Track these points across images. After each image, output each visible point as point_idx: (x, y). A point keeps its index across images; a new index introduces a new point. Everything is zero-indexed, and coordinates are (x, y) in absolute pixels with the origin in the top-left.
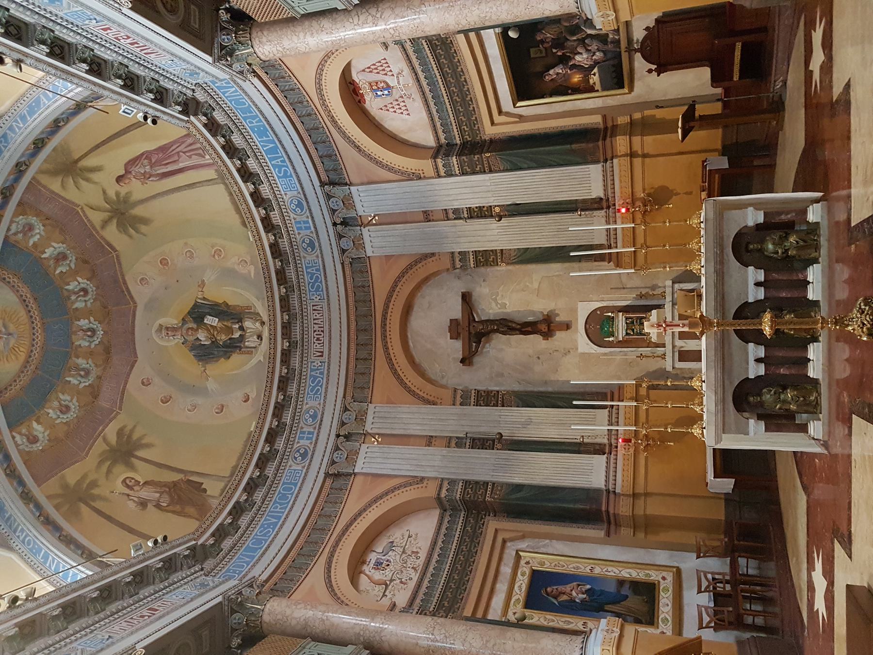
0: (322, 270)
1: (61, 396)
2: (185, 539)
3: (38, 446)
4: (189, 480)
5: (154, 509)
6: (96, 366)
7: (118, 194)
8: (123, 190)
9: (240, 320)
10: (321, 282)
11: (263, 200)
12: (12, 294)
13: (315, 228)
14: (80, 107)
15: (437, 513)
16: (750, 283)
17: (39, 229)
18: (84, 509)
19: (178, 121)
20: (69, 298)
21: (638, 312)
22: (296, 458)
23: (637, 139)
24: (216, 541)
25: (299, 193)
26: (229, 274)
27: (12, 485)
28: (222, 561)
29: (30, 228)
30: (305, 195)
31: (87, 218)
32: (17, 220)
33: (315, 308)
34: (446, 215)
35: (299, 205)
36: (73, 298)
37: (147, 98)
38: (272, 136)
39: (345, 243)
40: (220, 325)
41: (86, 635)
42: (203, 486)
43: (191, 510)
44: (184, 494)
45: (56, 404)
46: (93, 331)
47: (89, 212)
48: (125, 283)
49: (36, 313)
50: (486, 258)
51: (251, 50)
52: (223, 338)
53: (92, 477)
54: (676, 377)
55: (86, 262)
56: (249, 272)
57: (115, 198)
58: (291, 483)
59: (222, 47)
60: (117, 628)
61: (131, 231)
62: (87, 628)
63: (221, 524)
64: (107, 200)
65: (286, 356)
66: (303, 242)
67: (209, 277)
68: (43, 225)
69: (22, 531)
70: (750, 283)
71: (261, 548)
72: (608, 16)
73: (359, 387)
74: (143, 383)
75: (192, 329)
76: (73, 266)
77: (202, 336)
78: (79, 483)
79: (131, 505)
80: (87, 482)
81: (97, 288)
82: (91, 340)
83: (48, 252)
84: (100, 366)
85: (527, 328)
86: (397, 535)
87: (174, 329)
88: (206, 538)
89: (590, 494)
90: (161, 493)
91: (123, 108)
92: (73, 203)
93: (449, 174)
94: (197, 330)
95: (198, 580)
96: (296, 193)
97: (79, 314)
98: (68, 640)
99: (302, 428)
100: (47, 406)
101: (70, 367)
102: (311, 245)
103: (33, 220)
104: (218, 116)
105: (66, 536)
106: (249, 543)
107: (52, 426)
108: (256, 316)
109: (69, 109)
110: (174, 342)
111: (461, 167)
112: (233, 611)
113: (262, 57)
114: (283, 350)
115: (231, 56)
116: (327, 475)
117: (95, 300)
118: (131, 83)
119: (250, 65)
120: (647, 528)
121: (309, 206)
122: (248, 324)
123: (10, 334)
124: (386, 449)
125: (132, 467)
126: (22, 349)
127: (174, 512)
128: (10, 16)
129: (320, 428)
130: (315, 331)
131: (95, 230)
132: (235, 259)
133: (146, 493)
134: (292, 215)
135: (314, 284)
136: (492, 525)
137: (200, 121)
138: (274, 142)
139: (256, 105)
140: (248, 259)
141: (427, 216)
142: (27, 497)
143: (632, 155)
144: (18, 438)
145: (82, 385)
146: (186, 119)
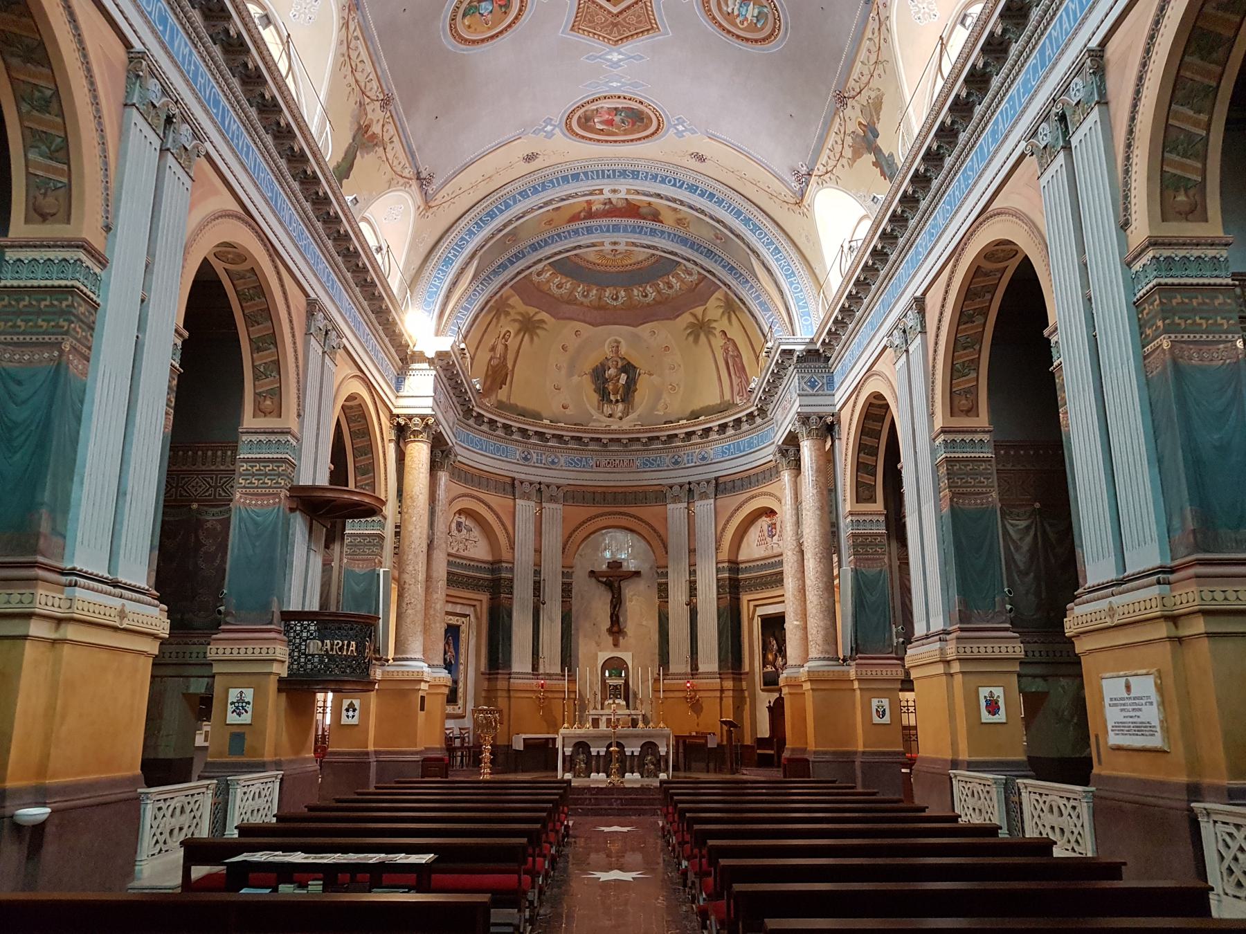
8: (717, 332)
15: (490, 558)
16: (633, 749)
21: (625, 693)
23: (731, 693)
26: (658, 397)
34: (692, 565)
35: (704, 458)
39: (676, 488)
46: (616, 299)
50: (663, 590)
54: (581, 716)
70: (633, 749)
72: (1112, 617)
73: (574, 495)
77: (612, 371)
78: (510, 306)
85: (615, 619)
86: (476, 533)
87: (617, 352)
89: (508, 664)
93: (718, 570)
102: (676, 463)
108: (626, 413)
110: (607, 351)
111: (722, 579)
112: (443, 452)
116: (513, 479)
120: (489, 696)
122: (621, 406)
124: (532, 520)
133: (500, 348)
136: (484, 597)
141: (692, 551)
143: (722, 691)
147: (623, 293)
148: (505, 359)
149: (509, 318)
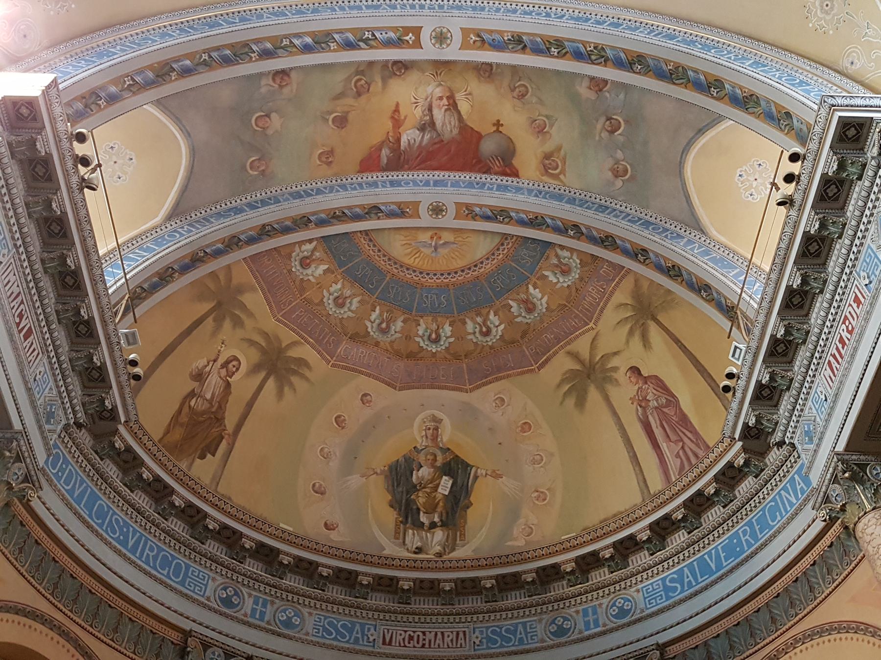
0: (521, 648)
1: (355, 301)
2: (130, 408)
3: (296, 266)
4: (223, 438)
5: (190, 389)
6: (392, 342)
7: (615, 369)
8: (621, 376)
9: (444, 525)
10: (502, 646)
11: (625, 558)
12: (484, 253)
13: (588, 638)
14: (730, 311)
17: (565, 281)
18: (207, 306)
19: (731, 424)
20: (479, 314)
22: (225, 589)
24: (119, 453)
25: (643, 611)
26: (513, 513)
27: (251, 229)
28: (85, 457)
29: (566, 272)
30: (639, 620)
31: (580, 334)
32: (575, 257)
33: (461, 635)
35: (623, 613)
36: (479, 320)
37: (760, 374)
38: (727, 565)
40: (439, 497)
41: (13, 238)
42: (209, 456)
43: (177, 435)
44: (203, 428)
45: (347, 292)
46: (437, 341)
47: (587, 338)
48: (498, 379)
49: (459, 278)
51: (869, 507)
52: (421, 499)
53: (248, 322)
55: (524, 334)
56: (516, 539)
57: (609, 366)
58: (186, 575)
59: (862, 467)
60: (12, 278)
61: (566, 387)
62: (24, 243)
63: (143, 463)
64: (606, 357)
65: (387, 585)
66: (565, 619)
67: (507, 484)
68: (568, 286)
69: (190, 231)
71: (90, 516)
74: (365, 395)
75: (435, 460)
76: (519, 319)
77: (425, 472)
78: (243, 307)
79: (201, 362)
80: (243, 316)
81: (491, 347)
82: (426, 338)
83: (535, 293)
84: (392, 347)
87: (435, 438)
88: (125, 437)
90: (210, 402)
91: (741, 346)
92: (598, 319)
94: (433, 466)
95: (61, 413)
96: (642, 606)
97: (458, 324)
98: (11, 213)
99: (273, 603)
100: (345, 282)
101: (392, 312)
103: (575, 275)
104: (747, 485)
105: (171, 276)
106: (104, 501)
107: (320, 286)
108: (450, 545)
109: (726, 298)
110: (417, 435)
113: (860, 526)
114: (398, 579)
115: (852, 478)
116: (187, 634)
117: (476, 344)
118: (781, 350)
119: (843, 509)
121: (622, 627)
122: (439, 535)
123: (436, 249)
125: (255, 369)
126: (417, 260)
127: (179, 411)
128: (852, 181)
129: (267, 631)
130: (424, 633)
131: (568, 343)
132: (533, 519)
133: (213, 383)
134: (605, 601)
135: (499, 635)
137: (736, 456)
138: (718, 570)
139: (774, 536)
140: (534, 537)
142: (233, 243)
144: (309, 247)
145: (369, 324)
146: (737, 436)
147: (448, 329)
148: (222, 406)
149: (240, 333)
